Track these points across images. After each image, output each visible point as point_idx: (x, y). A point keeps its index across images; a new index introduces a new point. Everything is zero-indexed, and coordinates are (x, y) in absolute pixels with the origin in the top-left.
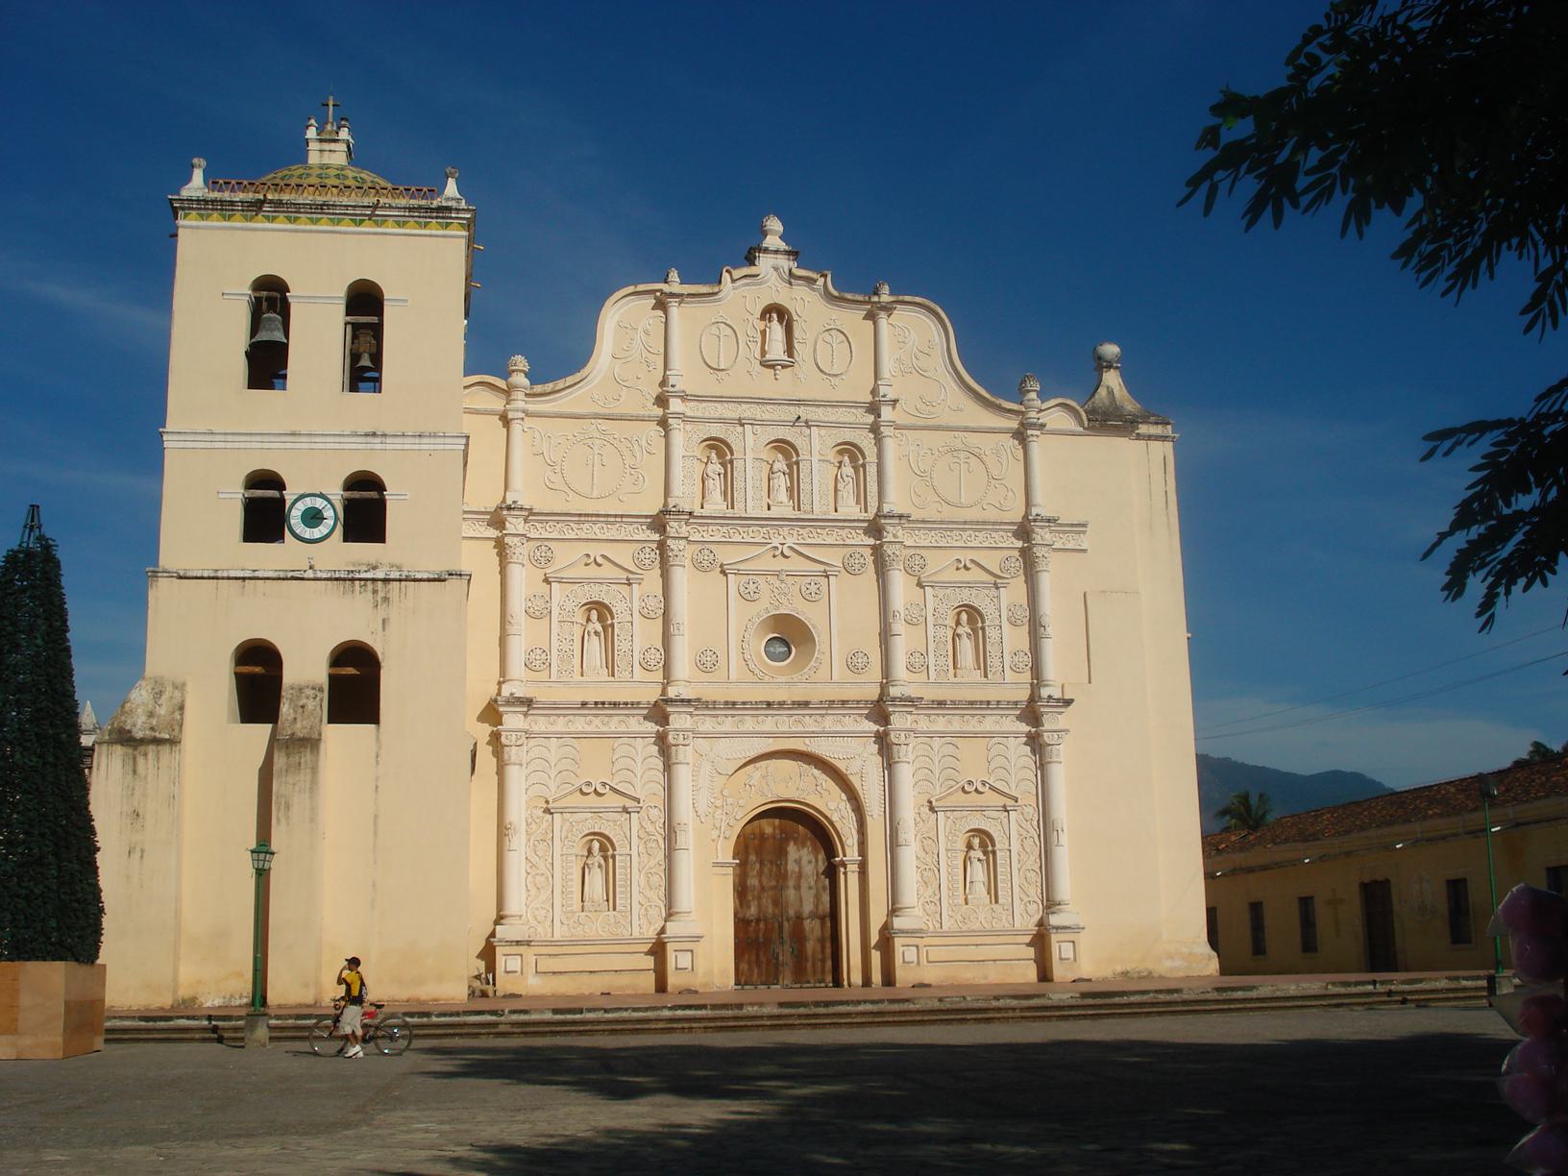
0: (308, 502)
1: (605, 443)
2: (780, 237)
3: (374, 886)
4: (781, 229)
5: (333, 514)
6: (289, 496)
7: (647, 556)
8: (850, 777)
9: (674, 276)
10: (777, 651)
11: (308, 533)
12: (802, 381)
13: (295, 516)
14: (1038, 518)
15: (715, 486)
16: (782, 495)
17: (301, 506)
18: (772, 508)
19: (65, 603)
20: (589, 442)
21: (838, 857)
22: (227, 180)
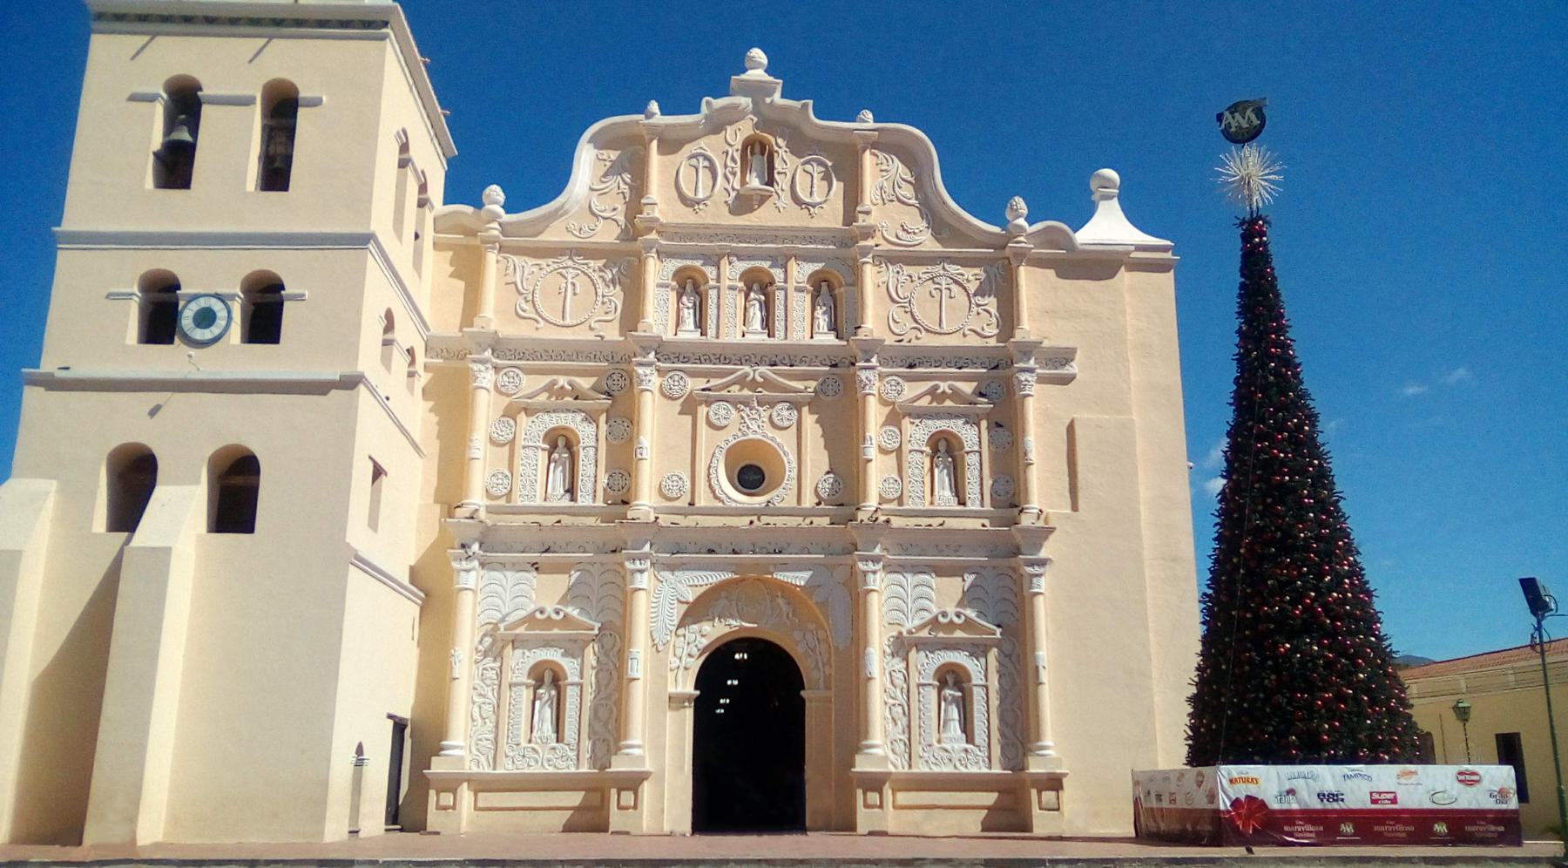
0: (215, 331)
1: (579, 272)
2: (766, 71)
3: (614, 551)
4: (765, 61)
5: (226, 315)
6: (185, 290)
7: (675, 484)
8: (142, 40)
9: (654, 106)
10: (751, 479)
11: (201, 334)
12: (776, 214)
13: (187, 319)
14: (1028, 350)
15: (689, 316)
16: (757, 324)
17: (194, 307)
18: (746, 335)
19: (1367, 582)
20: (564, 271)
21: (509, 208)
22: (692, 507)
